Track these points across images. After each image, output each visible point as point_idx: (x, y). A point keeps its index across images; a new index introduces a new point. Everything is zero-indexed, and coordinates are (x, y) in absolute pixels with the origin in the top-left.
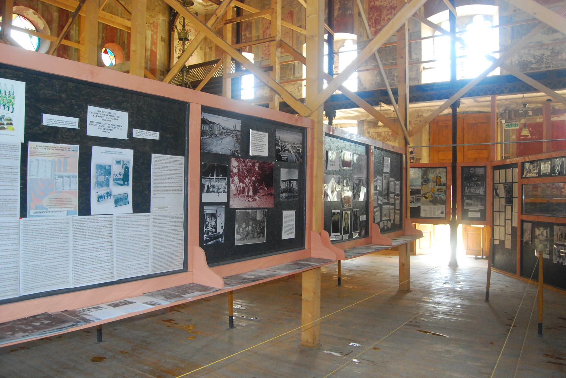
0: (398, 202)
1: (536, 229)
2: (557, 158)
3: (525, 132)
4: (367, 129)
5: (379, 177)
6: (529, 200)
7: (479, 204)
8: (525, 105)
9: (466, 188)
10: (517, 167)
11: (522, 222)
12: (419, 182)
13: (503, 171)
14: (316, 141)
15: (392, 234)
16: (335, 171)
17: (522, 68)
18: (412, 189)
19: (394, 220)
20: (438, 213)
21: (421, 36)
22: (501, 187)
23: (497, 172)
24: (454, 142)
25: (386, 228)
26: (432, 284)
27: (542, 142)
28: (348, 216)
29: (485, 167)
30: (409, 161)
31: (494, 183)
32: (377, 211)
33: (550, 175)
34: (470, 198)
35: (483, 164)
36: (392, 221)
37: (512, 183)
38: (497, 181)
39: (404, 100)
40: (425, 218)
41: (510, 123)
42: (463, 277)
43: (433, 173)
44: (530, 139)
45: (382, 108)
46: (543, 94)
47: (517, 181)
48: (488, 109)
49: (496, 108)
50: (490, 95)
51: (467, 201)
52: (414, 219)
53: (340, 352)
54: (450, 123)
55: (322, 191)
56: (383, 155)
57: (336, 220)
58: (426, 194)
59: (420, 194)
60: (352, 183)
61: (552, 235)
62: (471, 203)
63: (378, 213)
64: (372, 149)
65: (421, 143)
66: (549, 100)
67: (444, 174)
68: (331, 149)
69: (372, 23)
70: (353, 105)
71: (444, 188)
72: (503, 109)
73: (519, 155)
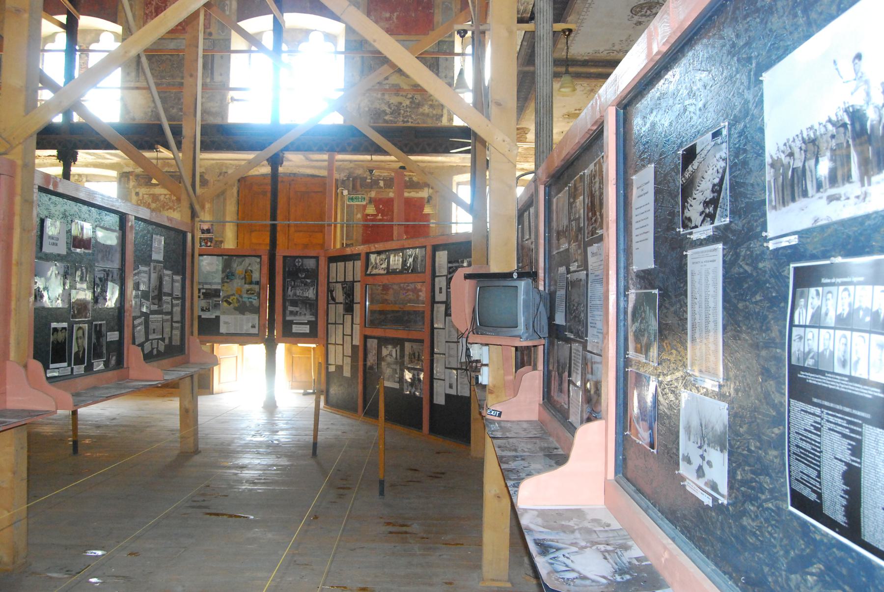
0: (177, 310)
1: (383, 347)
2: (409, 248)
3: (371, 210)
4: (134, 187)
5: (143, 268)
6: (378, 307)
7: (308, 312)
8: (371, 171)
9: (290, 288)
10: (360, 259)
11: (366, 338)
12: (218, 278)
13: (341, 265)
14: (18, 200)
15: (165, 362)
16: (59, 255)
17: (372, 118)
18: (206, 289)
19: (170, 339)
20: (246, 328)
21: (230, 47)
22: (339, 286)
23: (333, 266)
24: (274, 217)
25: (155, 352)
26: (235, 438)
27: (392, 226)
28: (813, 335)
29: (317, 258)
30: (197, 245)
31: (329, 283)
32: (140, 324)
33: (401, 272)
34: (294, 303)
35: (313, 254)
36: (167, 341)
37: (354, 281)
38: (333, 278)
39: (193, 146)
40: (228, 334)
41: (354, 196)
42: (284, 424)
43: (241, 264)
44: (380, 220)
45: (160, 155)
46: (393, 158)
47: (359, 279)
48: (324, 173)
49: (335, 172)
50: (328, 151)
51: (290, 308)
52: (205, 338)
53: (65, 570)
54: (269, 188)
55: (30, 288)
56: (151, 231)
57: (60, 341)
58: (229, 297)
59: (219, 296)
60: (92, 276)
61: (402, 356)
62: (297, 312)
63: (141, 329)
64: (131, 222)
65: (224, 215)
66: (403, 168)
67: (258, 266)
68: (50, 216)
69: (151, 12)
70: (106, 145)
71: (256, 287)
72: (345, 174)
73: (366, 241)
